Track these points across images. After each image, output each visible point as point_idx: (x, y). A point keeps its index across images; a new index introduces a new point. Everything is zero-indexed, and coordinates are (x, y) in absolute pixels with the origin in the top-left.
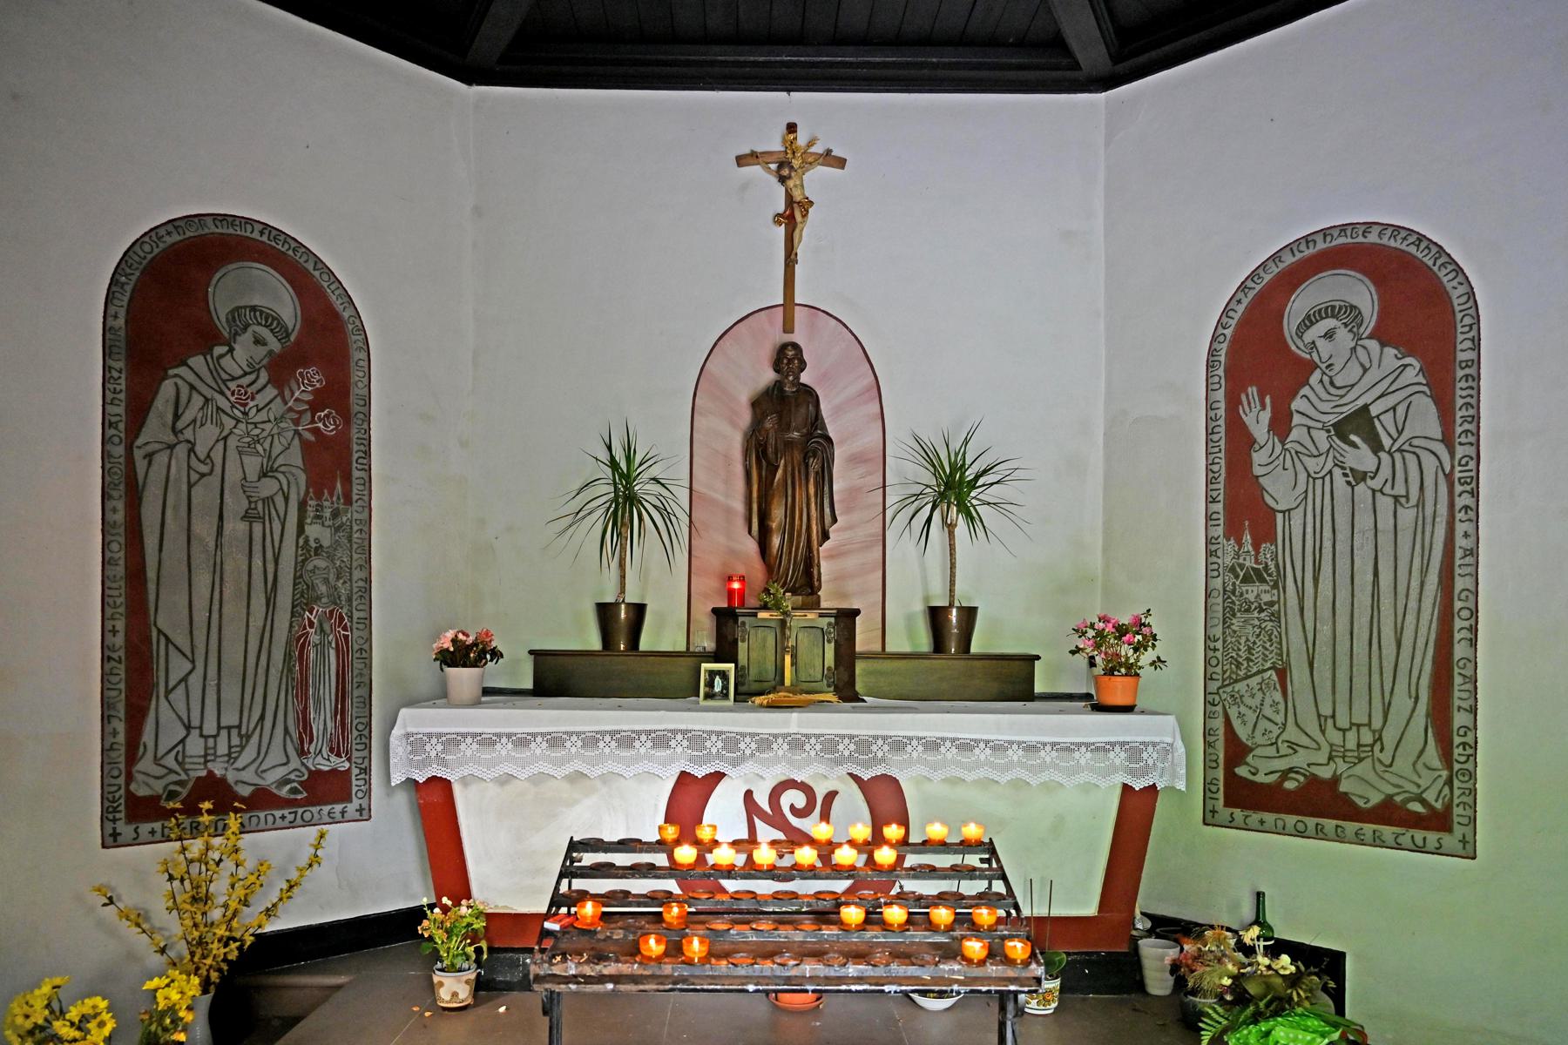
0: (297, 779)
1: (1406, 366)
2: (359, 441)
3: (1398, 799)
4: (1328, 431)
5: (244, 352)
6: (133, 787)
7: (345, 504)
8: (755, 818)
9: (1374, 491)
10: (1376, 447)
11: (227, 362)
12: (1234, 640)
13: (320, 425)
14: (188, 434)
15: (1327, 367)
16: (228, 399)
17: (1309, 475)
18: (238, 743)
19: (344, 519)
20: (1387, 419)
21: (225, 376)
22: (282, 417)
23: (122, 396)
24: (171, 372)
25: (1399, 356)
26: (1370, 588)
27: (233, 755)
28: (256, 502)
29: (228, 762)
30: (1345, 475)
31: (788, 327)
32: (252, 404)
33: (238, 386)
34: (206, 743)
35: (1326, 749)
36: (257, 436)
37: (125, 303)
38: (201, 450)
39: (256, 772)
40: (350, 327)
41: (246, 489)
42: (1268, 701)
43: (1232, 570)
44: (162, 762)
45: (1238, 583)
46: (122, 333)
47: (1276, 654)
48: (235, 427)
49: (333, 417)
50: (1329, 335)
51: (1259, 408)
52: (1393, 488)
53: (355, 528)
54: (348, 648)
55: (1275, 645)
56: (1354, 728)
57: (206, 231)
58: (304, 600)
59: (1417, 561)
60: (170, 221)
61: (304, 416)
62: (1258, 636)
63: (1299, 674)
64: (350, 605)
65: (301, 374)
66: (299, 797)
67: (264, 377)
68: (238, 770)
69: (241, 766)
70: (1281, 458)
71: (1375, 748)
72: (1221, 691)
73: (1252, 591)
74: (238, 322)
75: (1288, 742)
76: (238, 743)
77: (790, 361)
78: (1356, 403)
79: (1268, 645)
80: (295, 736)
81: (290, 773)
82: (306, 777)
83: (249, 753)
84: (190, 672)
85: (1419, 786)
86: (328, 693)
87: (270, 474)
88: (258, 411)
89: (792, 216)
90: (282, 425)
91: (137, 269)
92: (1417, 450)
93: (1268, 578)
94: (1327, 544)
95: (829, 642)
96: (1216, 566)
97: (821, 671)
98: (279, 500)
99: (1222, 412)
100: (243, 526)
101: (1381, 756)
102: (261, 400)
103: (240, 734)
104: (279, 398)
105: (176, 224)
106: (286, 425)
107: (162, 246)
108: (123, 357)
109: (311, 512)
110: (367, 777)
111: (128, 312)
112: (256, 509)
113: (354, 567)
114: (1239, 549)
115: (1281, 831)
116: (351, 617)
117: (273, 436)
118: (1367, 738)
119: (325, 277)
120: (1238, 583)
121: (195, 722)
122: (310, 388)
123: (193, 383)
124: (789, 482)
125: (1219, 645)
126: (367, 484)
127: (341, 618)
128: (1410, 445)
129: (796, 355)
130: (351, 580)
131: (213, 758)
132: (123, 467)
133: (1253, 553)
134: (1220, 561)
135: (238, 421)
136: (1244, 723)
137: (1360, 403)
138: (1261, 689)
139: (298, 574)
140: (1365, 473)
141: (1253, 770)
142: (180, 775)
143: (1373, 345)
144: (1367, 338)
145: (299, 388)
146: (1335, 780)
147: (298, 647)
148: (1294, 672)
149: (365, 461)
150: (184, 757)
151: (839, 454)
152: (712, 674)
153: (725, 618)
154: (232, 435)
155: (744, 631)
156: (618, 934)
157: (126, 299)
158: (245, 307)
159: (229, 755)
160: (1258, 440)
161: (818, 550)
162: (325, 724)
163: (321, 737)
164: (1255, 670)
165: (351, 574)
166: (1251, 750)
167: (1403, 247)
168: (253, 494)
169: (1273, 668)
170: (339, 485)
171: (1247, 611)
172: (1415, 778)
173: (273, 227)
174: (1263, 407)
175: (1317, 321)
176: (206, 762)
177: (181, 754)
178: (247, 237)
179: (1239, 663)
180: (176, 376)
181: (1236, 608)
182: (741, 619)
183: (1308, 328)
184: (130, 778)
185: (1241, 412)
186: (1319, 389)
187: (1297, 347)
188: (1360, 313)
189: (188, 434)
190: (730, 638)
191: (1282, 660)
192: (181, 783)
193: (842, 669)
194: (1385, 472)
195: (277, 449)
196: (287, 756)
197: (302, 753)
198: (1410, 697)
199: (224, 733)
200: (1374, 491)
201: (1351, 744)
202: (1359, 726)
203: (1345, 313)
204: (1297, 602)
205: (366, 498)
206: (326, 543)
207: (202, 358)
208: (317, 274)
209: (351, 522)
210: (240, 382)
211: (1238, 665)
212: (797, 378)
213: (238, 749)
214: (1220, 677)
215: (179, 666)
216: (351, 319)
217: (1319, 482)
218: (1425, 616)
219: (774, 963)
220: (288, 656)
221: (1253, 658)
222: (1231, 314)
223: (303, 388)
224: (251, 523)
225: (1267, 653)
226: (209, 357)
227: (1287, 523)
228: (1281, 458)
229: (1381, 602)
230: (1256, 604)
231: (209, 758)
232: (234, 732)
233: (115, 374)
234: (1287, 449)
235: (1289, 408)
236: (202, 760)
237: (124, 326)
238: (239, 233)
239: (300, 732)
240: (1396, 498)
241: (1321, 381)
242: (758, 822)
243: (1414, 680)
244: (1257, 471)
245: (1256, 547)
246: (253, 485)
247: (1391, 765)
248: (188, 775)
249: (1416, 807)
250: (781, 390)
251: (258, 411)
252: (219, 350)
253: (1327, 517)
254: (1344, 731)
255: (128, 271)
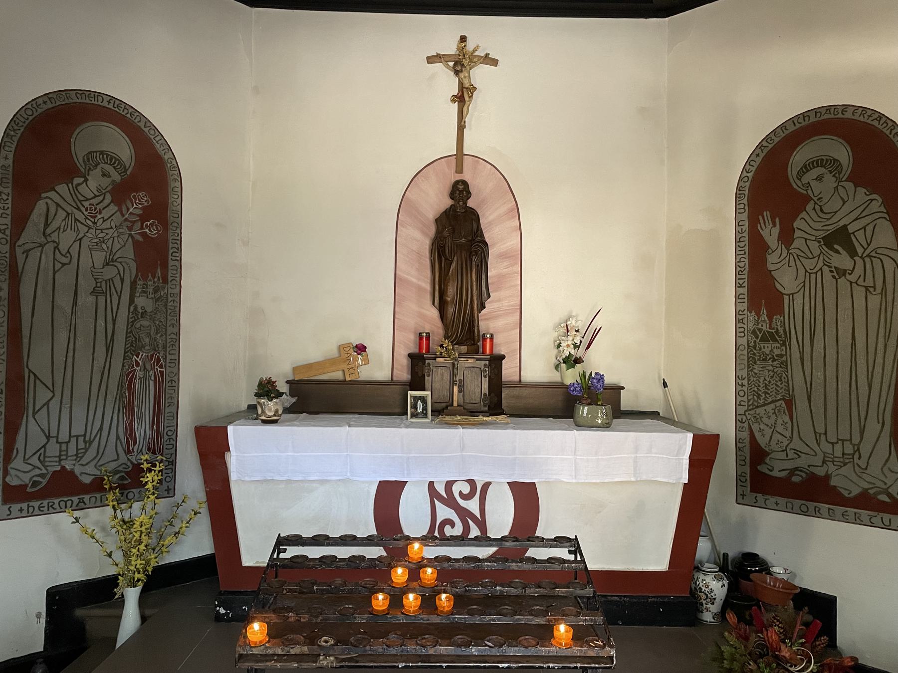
0: (124, 470)
1: (872, 200)
2: (174, 241)
3: (871, 492)
4: (819, 242)
5: (94, 183)
6: (8, 479)
7: (162, 283)
8: (435, 500)
9: (851, 283)
10: (853, 253)
11: (83, 189)
12: (755, 379)
13: (147, 230)
14: (54, 237)
15: (818, 200)
16: (84, 214)
17: (806, 271)
18: (83, 447)
19: (162, 293)
20: (860, 235)
21: (81, 198)
22: (120, 225)
23: (9, 212)
24: (43, 195)
25: (868, 193)
26: (850, 348)
27: (79, 455)
28: (101, 282)
29: (75, 460)
30: (831, 271)
31: (459, 169)
32: (99, 216)
33: (90, 205)
34: (61, 447)
35: (820, 456)
36: (103, 238)
37: (13, 149)
38: (63, 247)
39: (95, 466)
40: (169, 165)
41: (94, 274)
42: (780, 421)
43: (754, 332)
44: (29, 461)
45: (758, 341)
46: (11, 169)
47: (785, 390)
48: (87, 232)
49: (156, 225)
50: (819, 178)
51: (771, 225)
52: (864, 281)
53: (170, 299)
54: (162, 379)
55: (784, 384)
56: (840, 442)
57: (71, 101)
58: (133, 348)
59: (882, 331)
60: (45, 94)
61: (136, 225)
62: (772, 377)
63: (801, 404)
64: (165, 351)
65: (134, 196)
66: (126, 482)
67: (108, 198)
68: (82, 465)
69: (84, 463)
70: (787, 259)
71: (855, 456)
72: (747, 413)
73: (767, 348)
74: (91, 162)
75: (795, 450)
76: (83, 447)
77: (461, 192)
78: (838, 224)
79: (779, 384)
80: (124, 441)
81: (120, 466)
82: (130, 469)
83: (91, 453)
84: (51, 399)
85: (885, 484)
86: (148, 412)
87: (111, 263)
88: (104, 221)
89: (463, 97)
90: (120, 230)
91: (22, 126)
92: (881, 257)
93: (778, 339)
94: (820, 318)
95: (485, 377)
96: (742, 330)
97: (480, 396)
98: (117, 281)
99: (746, 228)
100: (92, 299)
101: (860, 463)
102: (106, 214)
103: (85, 441)
104: (118, 213)
105: (50, 96)
106: (123, 231)
107: (40, 111)
108: (10, 185)
109: (139, 289)
110: (174, 467)
111: (14, 156)
112: (101, 287)
113: (168, 325)
114: (759, 319)
115: (791, 511)
116: (165, 359)
117: (114, 238)
118: (849, 449)
119: (152, 132)
120: (758, 341)
121: (54, 433)
122: (140, 206)
123: (58, 202)
124: (460, 271)
125: (745, 382)
126: (179, 270)
127: (159, 360)
128: (876, 253)
129: (464, 188)
130: (166, 334)
131: (64, 457)
132: (8, 260)
133: (768, 322)
134: (745, 326)
135: (90, 228)
136: (763, 435)
137: (841, 223)
138: (775, 413)
139: (129, 330)
140: (845, 270)
141: (770, 468)
142: (41, 470)
143: (850, 186)
144: (846, 181)
145: (133, 205)
146: (827, 477)
147: (128, 380)
148: (797, 402)
149: (177, 255)
150: (45, 457)
151: (492, 252)
152: (416, 399)
153: (417, 361)
154: (85, 238)
155: (429, 369)
156: (304, 618)
157: (14, 147)
158: (96, 152)
159: (77, 455)
160: (771, 247)
161: (478, 315)
162: (145, 432)
163: (142, 440)
164: (770, 400)
165: (166, 330)
166: (768, 454)
167: (869, 121)
168: (98, 277)
169: (783, 399)
170: (159, 270)
171: (764, 360)
172: (884, 479)
173: (116, 99)
174: (774, 225)
175: (811, 169)
176: (60, 460)
177: (42, 456)
178: (99, 105)
179: (759, 394)
180: (47, 197)
181: (757, 358)
182: (427, 361)
183: (805, 173)
184: (6, 473)
185: (759, 228)
186: (812, 213)
187: (798, 186)
188: (840, 164)
189: (54, 237)
190: (420, 374)
191: (789, 395)
192: (42, 476)
193: (493, 395)
194: (859, 270)
195: (117, 246)
196: (118, 455)
197: (128, 452)
198: (879, 422)
199: (74, 440)
200: (851, 283)
201: (838, 453)
202: (843, 441)
203: (830, 164)
204: (799, 355)
205: (178, 279)
206: (149, 310)
207: (65, 185)
208: (146, 130)
209: (167, 295)
210: (91, 202)
211: (759, 396)
212: (466, 203)
213: (84, 451)
214: (746, 404)
215: (43, 395)
216: (170, 160)
217: (813, 276)
218: (888, 367)
219: (417, 644)
220: (120, 386)
221: (769, 392)
222: (752, 163)
223: (135, 206)
224: (97, 297)
225: (778, 389)
226: (70, 185)
227: (791, 303)
228: (787, 259)
229: (858, 357)
230: (770, 356)
231: (62, 457)
232: (81, 439)
233: (5, 197)
234: (791, 253)
235: (793, 225)
236: (57, 459)
237: (11, 165)
238: (93, 102)
239: (127, 438)
240: (867, 288)
241: (814, 209)
242: (436, 502)
243: (881, 411)
244: (771, 267)
245: (770, 318)
246: (98, 271)
247: (866, 469)
248: (47, 470)
249: (884, 498)
250: (455, 211)
251: (104, 221)
252: (77, 180)
253: (819, 299)
254: (833, 444)
255: (16, 127)
